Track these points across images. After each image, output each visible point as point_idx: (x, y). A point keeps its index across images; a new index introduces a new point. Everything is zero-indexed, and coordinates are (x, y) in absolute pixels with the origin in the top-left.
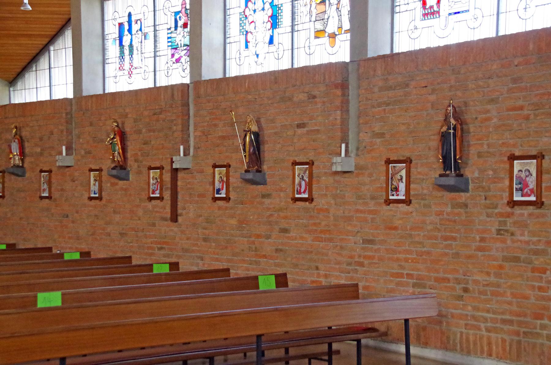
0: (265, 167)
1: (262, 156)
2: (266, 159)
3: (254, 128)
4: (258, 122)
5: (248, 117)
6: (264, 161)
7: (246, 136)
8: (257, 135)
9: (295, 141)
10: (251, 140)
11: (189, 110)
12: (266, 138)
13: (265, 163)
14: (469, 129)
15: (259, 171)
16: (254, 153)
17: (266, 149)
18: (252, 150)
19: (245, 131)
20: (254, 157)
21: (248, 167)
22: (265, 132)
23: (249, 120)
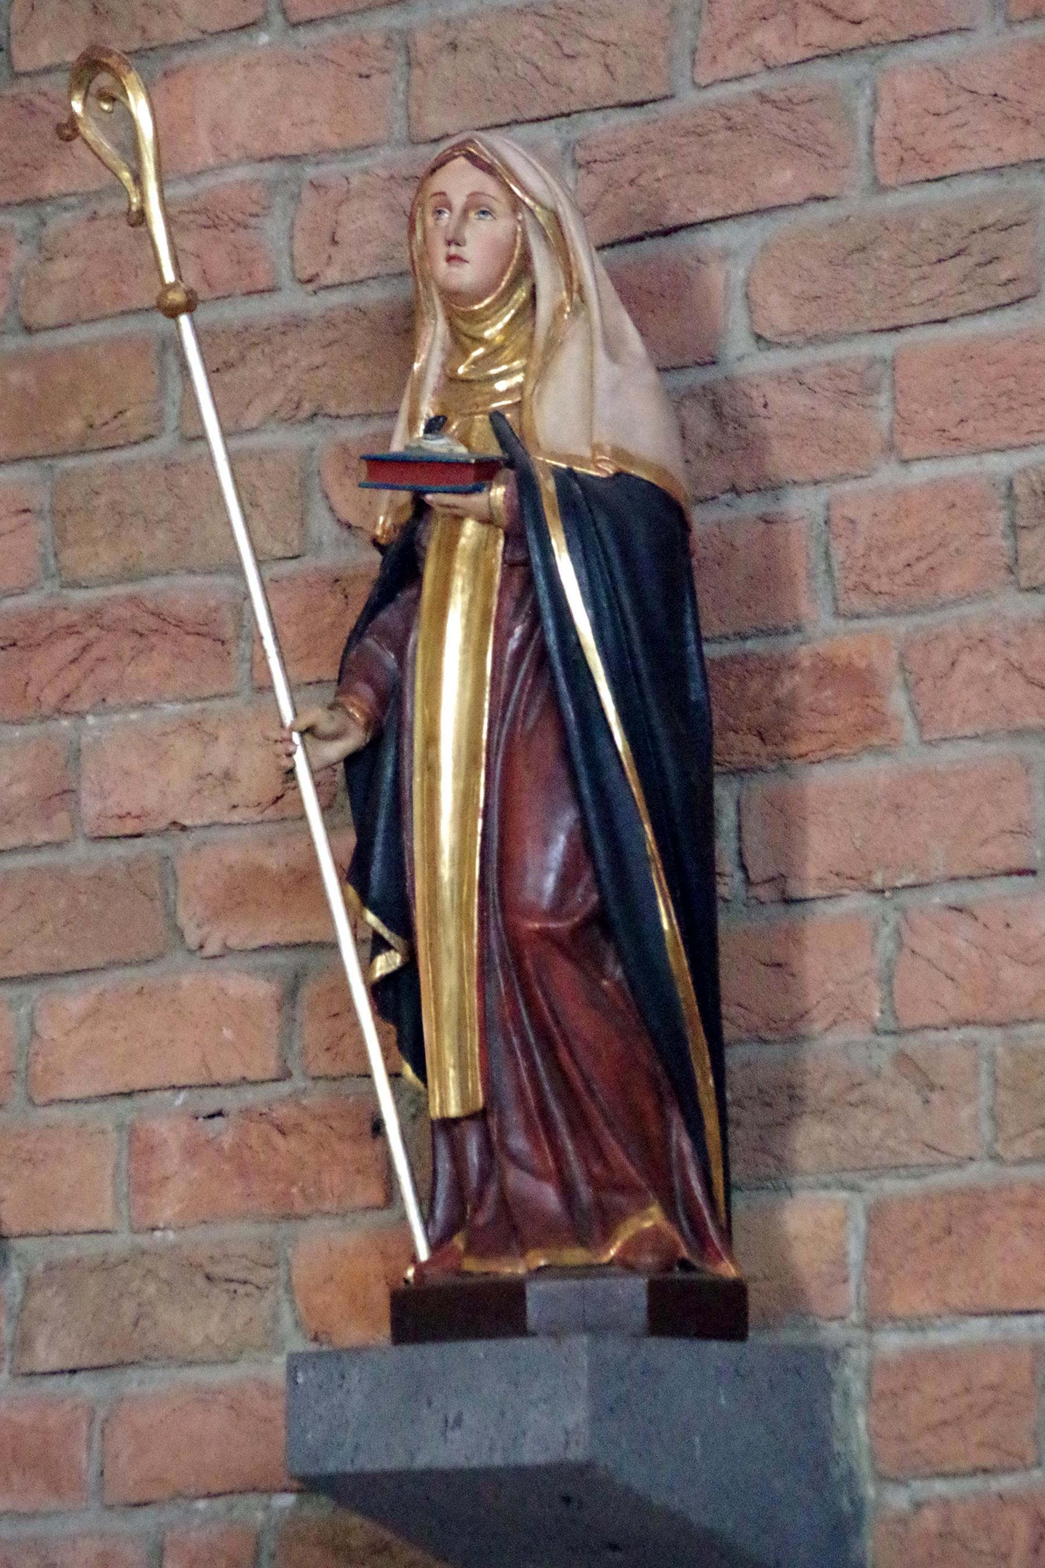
0: (814, 1226)
1: (734, 979)
2: (836, 1046)
3: (591, 405)
4: (651, 263)
5: (460, 181)
6: (786, 1101)
7: (401, 569)
8: (643, 539)
9: (722, 712)
10: (534, 664)
11: (161, 191)
12: (823, 627)
13: (809, 1139)
14: (793, 693)
15: (700, 1307)
16: (609, 923)
17: (821, 850)
18: (546, 865)
19: (383, 468)
20: (584, 1006)
21: (470, 1209)
22: (802, 504)
23: (482, 242)
